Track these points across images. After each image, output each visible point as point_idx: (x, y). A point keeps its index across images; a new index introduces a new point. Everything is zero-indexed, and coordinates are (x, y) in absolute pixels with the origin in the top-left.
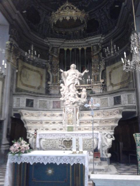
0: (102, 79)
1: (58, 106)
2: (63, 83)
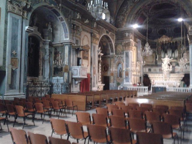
1: (161, 71)
2: (163, 63)
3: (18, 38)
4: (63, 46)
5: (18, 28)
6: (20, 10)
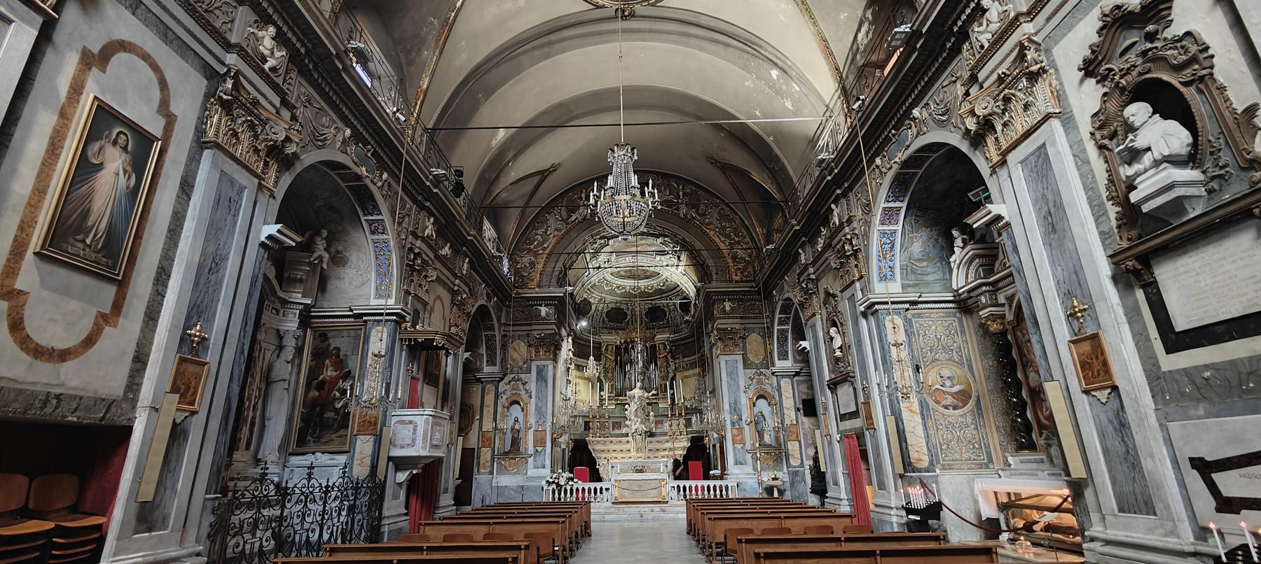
3: (225, 269)
4: (361, 320)
5: (236, 223)
6: (257, 151)
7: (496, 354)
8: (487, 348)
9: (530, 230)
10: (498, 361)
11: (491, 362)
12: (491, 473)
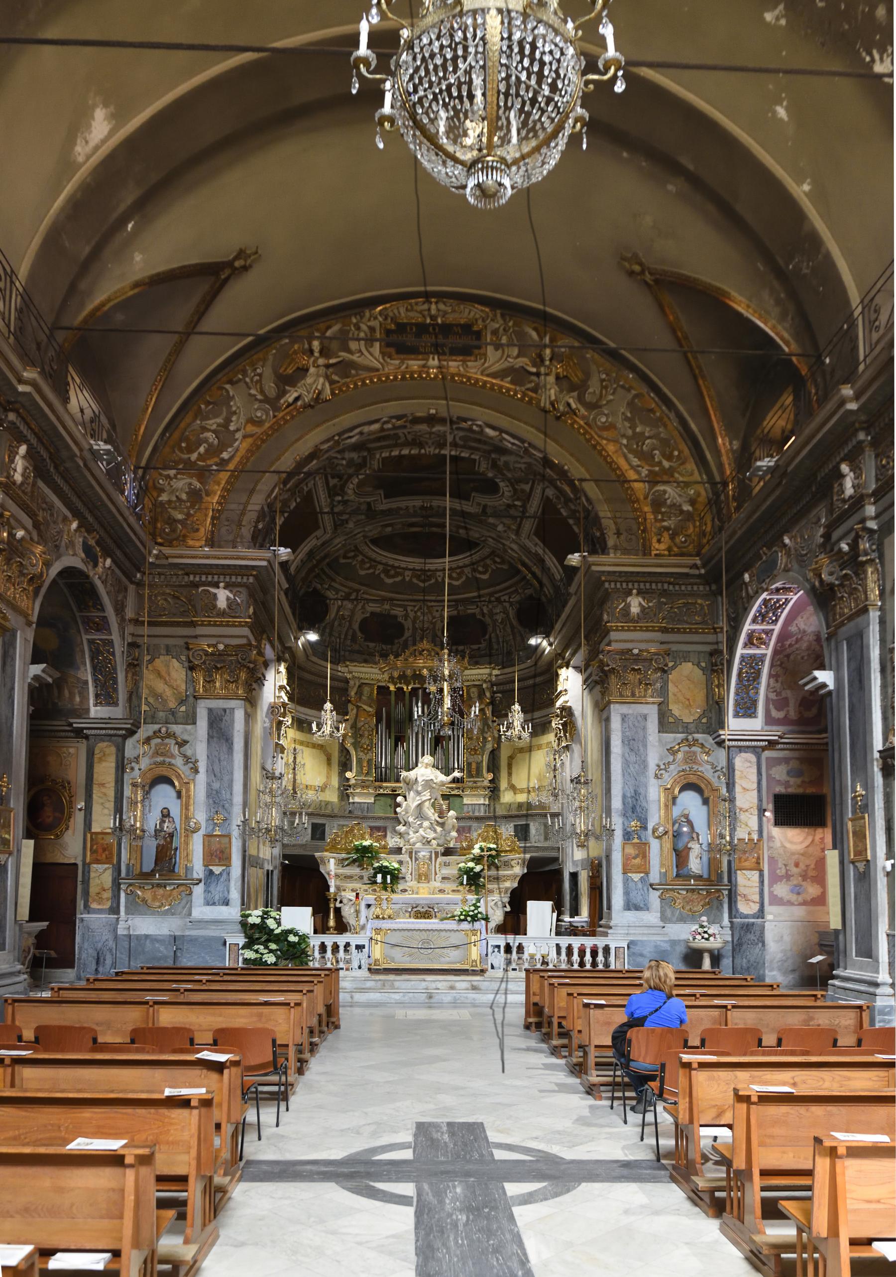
0: (489, 771)
7: (115, 681)
8: (94, 668)
9: (188, 419)
10: (122, 695)
11: (107, 696)
12: (115, 910)
